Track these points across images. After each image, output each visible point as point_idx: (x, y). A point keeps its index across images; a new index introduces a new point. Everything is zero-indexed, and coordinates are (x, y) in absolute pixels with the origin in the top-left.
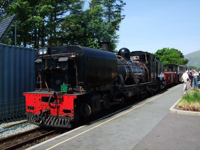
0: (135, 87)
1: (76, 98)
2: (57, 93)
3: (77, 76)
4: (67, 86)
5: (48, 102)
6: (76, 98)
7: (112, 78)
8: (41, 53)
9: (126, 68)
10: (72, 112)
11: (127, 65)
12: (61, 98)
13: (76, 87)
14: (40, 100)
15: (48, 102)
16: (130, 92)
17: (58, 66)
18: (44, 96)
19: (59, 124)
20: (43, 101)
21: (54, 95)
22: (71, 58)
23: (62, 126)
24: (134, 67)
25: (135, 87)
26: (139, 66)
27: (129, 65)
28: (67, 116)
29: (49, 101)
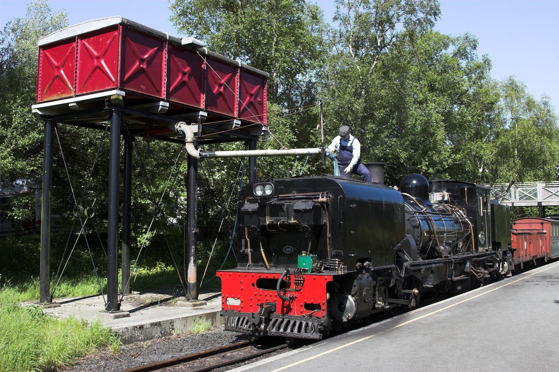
0: (441, 264)
1: (332, 280)
2: (292, 270)
3: (329, 238)
4: (312, 257)
5: (275, 288)
6: (332, 280)
7: (106, 296)
8: (259, 193)
9: (421, 220)
10: (324, 307)
11: (423, 213)
12: (301, 281)
13: (327, 260)
14: (253, 285)
15: (275, 288)
16: (431, 275)
17: (292, 219)
18: (264, 277)
19: (296, 330)
20: (259, 286)
21: (286, 275)
22: (318, 202)
23: (303, 335)
24: (438, 218)
25: (441, 264)
26: (449, 215)
27: (428, 215)
28: (310, 316)
29: (278, 287)
